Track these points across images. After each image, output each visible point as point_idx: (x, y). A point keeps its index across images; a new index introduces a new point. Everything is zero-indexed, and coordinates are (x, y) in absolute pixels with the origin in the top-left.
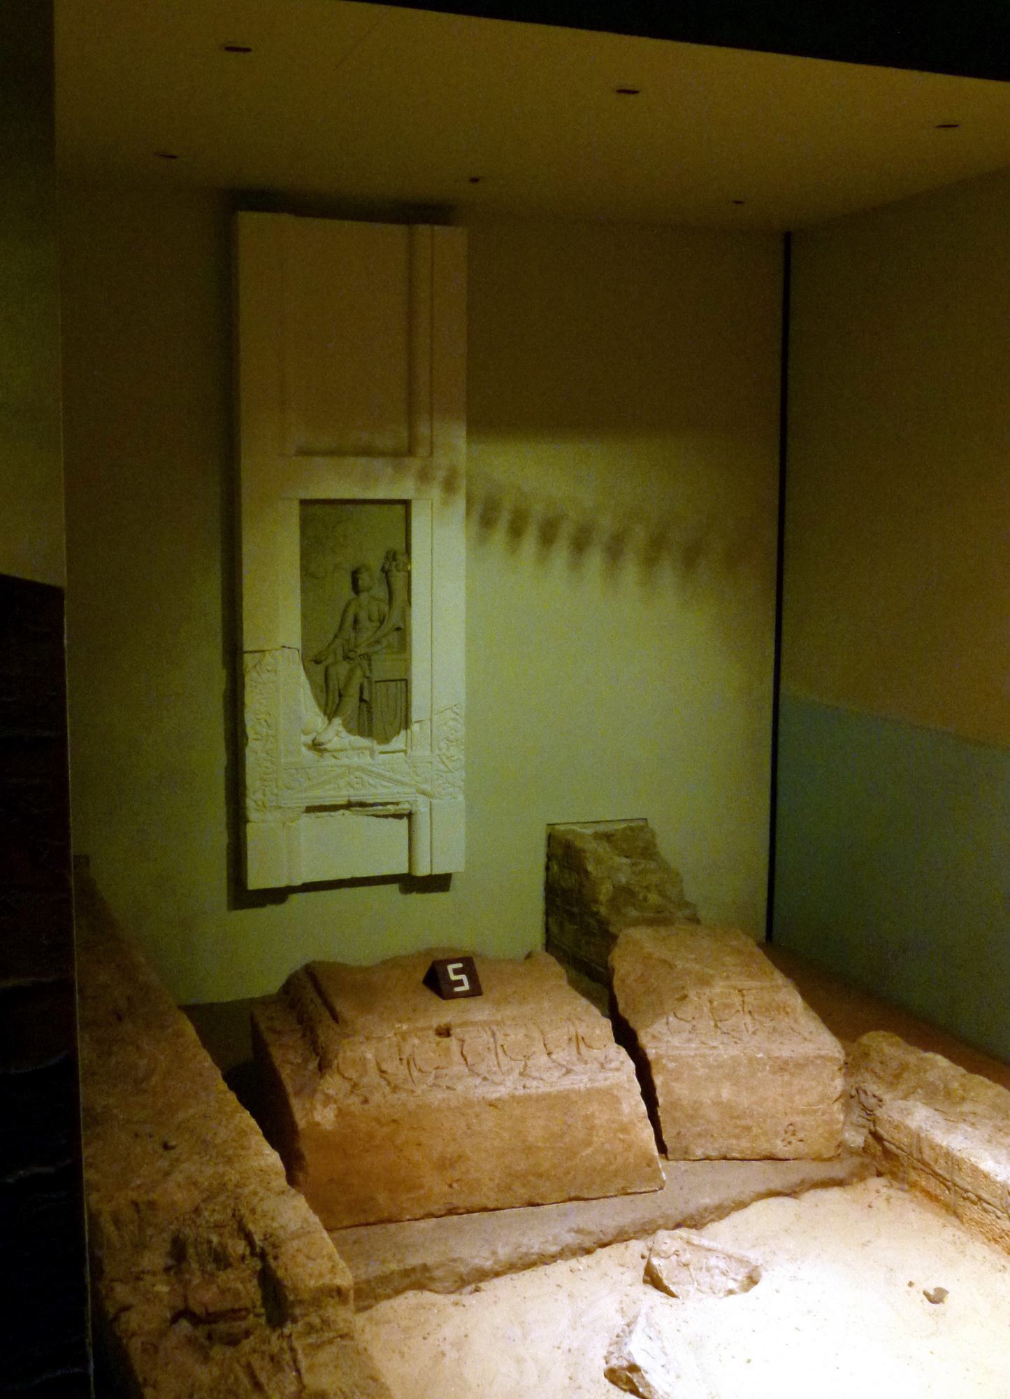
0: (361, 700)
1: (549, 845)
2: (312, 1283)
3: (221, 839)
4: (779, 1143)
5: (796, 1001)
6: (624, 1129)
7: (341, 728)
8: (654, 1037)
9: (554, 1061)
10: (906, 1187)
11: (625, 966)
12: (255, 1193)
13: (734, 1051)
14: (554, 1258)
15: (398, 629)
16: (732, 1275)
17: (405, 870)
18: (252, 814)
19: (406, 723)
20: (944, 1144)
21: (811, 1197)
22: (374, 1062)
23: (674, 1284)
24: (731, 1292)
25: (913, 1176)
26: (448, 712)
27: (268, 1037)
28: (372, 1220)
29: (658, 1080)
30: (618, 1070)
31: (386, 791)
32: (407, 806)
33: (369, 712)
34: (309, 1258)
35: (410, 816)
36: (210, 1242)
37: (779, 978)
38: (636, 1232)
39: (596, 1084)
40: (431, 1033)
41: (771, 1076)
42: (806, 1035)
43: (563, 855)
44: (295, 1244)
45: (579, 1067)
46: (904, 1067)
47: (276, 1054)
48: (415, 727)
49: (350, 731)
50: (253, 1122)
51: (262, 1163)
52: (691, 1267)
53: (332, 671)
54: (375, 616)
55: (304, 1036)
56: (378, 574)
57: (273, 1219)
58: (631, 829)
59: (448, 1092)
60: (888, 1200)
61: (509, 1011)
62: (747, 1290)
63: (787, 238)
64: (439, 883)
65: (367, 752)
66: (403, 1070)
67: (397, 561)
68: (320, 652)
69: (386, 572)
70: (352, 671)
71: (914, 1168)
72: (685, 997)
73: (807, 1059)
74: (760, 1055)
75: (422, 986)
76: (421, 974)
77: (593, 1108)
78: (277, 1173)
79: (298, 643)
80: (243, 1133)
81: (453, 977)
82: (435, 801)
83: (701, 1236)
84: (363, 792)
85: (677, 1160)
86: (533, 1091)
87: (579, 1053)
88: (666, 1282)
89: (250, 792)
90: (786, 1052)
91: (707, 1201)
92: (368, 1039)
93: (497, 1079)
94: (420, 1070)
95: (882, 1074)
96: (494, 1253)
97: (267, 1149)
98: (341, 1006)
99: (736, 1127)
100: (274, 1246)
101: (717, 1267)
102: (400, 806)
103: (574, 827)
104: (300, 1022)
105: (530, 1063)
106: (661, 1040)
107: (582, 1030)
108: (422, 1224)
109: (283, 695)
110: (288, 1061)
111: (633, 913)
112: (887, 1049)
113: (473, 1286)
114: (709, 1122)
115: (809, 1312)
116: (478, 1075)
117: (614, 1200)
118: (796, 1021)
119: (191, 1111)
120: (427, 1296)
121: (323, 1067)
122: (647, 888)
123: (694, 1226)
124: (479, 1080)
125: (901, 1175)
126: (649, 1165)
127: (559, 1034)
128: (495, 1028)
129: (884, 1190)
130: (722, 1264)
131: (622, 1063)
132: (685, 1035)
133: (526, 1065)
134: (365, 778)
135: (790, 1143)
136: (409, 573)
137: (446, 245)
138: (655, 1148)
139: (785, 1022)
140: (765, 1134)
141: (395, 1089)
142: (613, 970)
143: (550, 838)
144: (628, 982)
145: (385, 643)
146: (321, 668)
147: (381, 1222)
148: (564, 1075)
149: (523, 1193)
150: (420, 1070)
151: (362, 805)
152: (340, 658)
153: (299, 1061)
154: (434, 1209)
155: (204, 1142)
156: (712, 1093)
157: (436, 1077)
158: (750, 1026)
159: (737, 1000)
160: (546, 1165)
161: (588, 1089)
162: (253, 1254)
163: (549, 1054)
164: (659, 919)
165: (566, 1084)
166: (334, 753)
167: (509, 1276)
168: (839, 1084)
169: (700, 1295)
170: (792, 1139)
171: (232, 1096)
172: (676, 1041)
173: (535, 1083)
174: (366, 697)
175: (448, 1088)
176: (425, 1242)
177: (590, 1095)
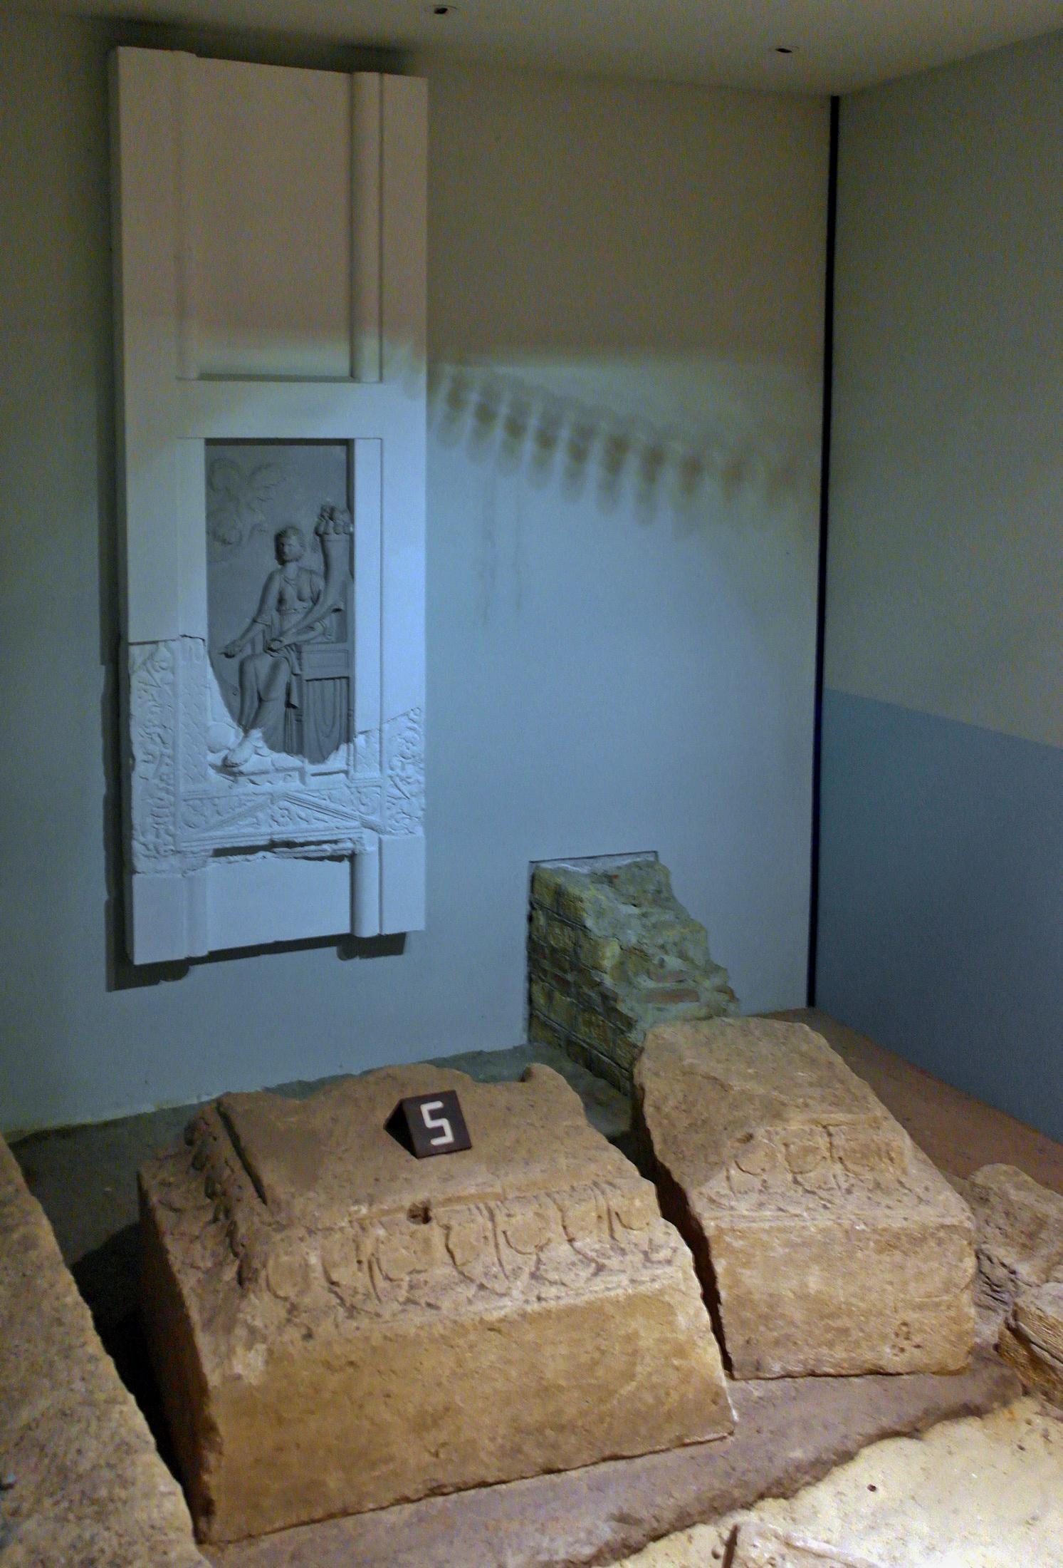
0: (289, 705)
1: (532, 889)
3: (100, 894)
5: (903, 1142)
6: (680, 1351)
7: (261, 744)
8: (712, 1201)
9: (578, 1252)
13: (825, 1220)
15: (338, 610)
18: (140, 862)
19: (348, 736)
22: (319, 1269)
26: (404, 719)
27: (164, 1218)
29: (720, 1266)
31: (321, 825)
32: (349, 845)
33: (299, 721)
35: (352, 857)
38: (702, 1513)
39: (642, 1289)
40: (402, 1216)
41: (875, 1257)
42: (920, 1191)
43: (551, 906)
45: (614, 1262)
47: (175, 1251)
48: (360, 740)
49: (273, 747)
53: (249, 668)
54: (307, 592)
55: (215, 1220)
56: (309, 536)
58: (637, 865)
61: (514, 1177)
63: (835, 102)
64: (392, 944)
65: (296, 774)
67: (336, 519)
68: (233, 643)
69: (320, 535)
70: (275, 667)
72: (750, 1137)
73: (924, 1228)
75: (385, 1134)
77: (637, 1323)
78: (178, 1529)
79: (202, 630)
80: (125, 1449)
81: (430, 1124)
82: (385, 838)
84: (291, 827)
85: (746, 1379)
86: (552, 1303)
87: (613, 1237)
89: (137, 834)
91: (798, 1454)
92: (311, 1232)
93: (499, 1286)
94: (388, 1278)
95: (1010, 1230)
98: (269, 1176)
99: (828, 1329)
102: (341, 846)
104: (211, 1195)
105: (543, 1256)
106: (722, 1204)
107: (616, 1202)
109: (182, 699)
110: (191, 1259)
111: (648, 984)
114: (792, 1323)
116: (472, 1281)
118: (904, 1172)
119: (43, 1404)
122: (663, 947)
124: (471, 1291)
126: (715, 1402)
127: (583, 1211)
128: (492, 1204)
129: (1038, 1420)
132: (754, 1198)
133: (539, 1261)
134: (294, 808)
135: (902, 1350)
136: (352, 535)
137: (399, 99)
139: (889, 1174)
140: (869, 1337)
141: (352, 1311)
142: (643, 1089)
143: (533, 879)
144: (666, 1110)
145: (319, 627)
146: (234, 663)
147: (331, 1516)
148: (595, 1274)
149: (539, 1457)
150: (388, 1278)
151: (289, 844)
152: (259, 648)
153: (209, 1264)
155: (63, 1472)
156: (794, 1283)
157: (412, 1287)
158: (841, 1179)
159: (822, 1141)
160: (571, 1411)
161: (629, 1298)
163: (571, 1241)
166: (252, 777)
170: (905, 1344)
171: (108, 1365)
172: (743, 1207)
173: (553, 1291)
174: (295, 701)
177: (631, 1305)
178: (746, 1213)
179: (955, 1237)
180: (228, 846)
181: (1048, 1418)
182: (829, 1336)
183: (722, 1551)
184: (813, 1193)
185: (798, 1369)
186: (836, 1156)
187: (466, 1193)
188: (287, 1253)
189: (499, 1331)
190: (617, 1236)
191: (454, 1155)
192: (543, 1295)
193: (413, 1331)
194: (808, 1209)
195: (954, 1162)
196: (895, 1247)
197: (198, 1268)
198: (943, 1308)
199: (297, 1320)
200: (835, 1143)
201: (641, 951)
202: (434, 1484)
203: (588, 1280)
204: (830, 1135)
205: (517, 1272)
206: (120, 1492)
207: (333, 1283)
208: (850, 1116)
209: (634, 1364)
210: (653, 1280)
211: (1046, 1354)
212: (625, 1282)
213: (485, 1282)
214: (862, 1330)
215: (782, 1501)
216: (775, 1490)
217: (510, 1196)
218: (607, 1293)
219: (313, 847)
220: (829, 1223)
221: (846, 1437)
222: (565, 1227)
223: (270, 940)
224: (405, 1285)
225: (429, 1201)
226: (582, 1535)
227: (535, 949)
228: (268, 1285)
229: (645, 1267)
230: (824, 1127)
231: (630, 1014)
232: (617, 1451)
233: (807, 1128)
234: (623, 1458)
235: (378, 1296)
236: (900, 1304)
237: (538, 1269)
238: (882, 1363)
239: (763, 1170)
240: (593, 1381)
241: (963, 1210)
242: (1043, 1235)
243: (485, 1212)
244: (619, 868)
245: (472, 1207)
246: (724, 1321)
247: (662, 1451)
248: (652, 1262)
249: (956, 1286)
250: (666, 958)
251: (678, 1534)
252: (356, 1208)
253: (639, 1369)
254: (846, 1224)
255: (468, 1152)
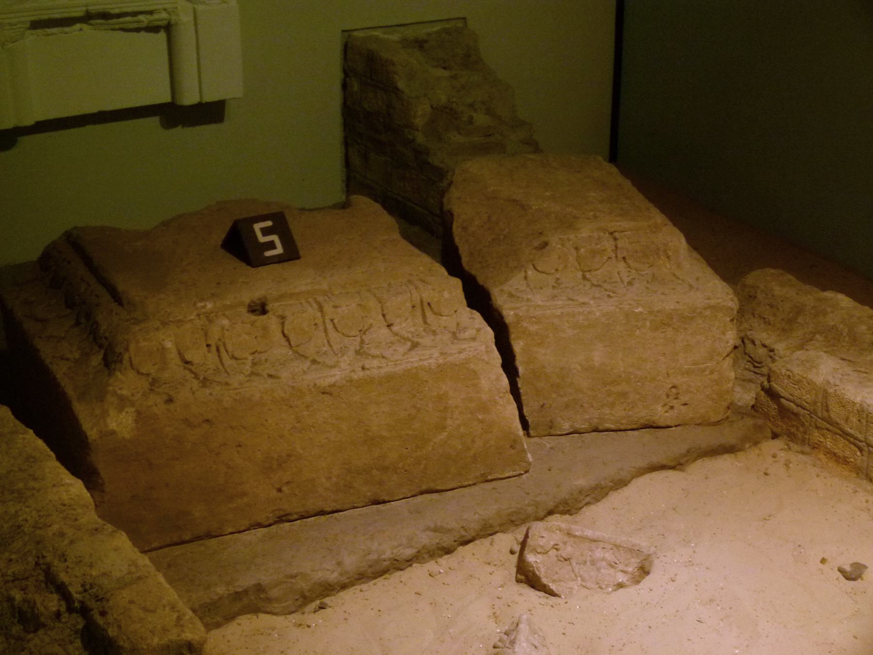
2: (156, 641)
4: (659, 408)
5: (677, 241)
6: (484, 408)
8: (511, 295)
10: (807, 449)
11: (466, 211)
12: (62, 535)
14: (409, 562)
16: (621, 567)
17: (166, 98)
20: (858, 400)
21: (699, 468)
22: (174, 351)
23: (554, 581)
24: (620, 586)
25: (816, 436)
28: (187, 538)
29: (518, 346)
30: (474, 339)
32: (164, 15)
34: (146, 610)
35: (168, 28)
36: (10, 599)
37: (659, 218)
38: (501, 525)
40: (244, 310)
43: (365, 72)
44: (126, 595)
45: (426, 340)
46: (799, 310)
47: (46, 351)
50: (40, 443)
51: (65, 496)
52: (574, 562)
55: (78, 324)
57: (91, 566)
58: (447, 31)
59: (270, 381)
60: (787, 465)
62: (638, 582)
64: (210, 113)
66: (212, 358)
71: (817, 428)
72: (546, 244)
74: (640, 309)
75: (222, 252)
76: (219, 235)
81: (262, 239)
83: (576, 523)
85: (540, 436)
86: (375, 372)
87: (425, 322)
88: (545, 581)
90: (669, 305)
91: (581, 482)
92: (164, 324)
94: (233, 357)
95: (772, 319)
96: (339, 564)
97: (68, 478)
100: (99, 599)
101: (603, 559)
102: (156, 16)
103: (375, 33)
105: (366, 338)
107: (427, 294)
108: (247, 537)
110: (62, 356)
111: (456, 138)
112: (778, 291)
113: (318, 602)
115: (711, 600)
116: (306, 358)
117: (473, 489)
118: (679, 266)
120: (264, 620)
121: (111, 360)
122: (471, 106)
123: (568, 512)
124: (308, 363)
125: (800, 436)
128: (320, 299)
130: (609, 556)
131: (479, 330)
133: (362, 342)
135: (672, 407)
138: (519, 426)
141: (205, 382)
142: (452, 215)
143: (346, 48)
147: (199, 538)
150: (233, 357)
151: (105, 16)
153: (77, 355)
154: (262, 518)
157: (254, 364)
159: (608, 244)
162: (70, 610)
164: (489, 146)
165: (414, 360)
167: (358, 587)
168: (731, 337)
169: (585, 592)
170: (674, 403)
172: (538, 299)
173: (376, 363)
175: (270, 376)
176: (250, 554)
178: (540, 303)
179: (720, 315)
180: (45, 17)
181: (790, 452)
182: (611, 399)
183: (517, 548)
184: (598, 286)
185: (585, 426)
186: (620, 256)
187: (297, 290)
188: (144, 340)
189: (331, 394)
190: (429, 321)
191: (286, 264)
192: (367, 366)
193: (258, 396)
194: (594, 298)
195: (729, 269)
196: (669, 325)
197: (67, 359)
198: (707, 372)
199: (160, 390)
200: (619, 246)
201: (452, 109)
202: (282, 513)
203: (405, 354)
204: (615, 239)
205: (343, 351)
206: (32, 484)
207: (187, 362)
208: (632, 223)
209: (445, 419)
210: (460, 353)
211: (792, 404)
212: (436, 355)
213: (317, 358)
214: (638, 393)
215: (567, 516)
216: (561, 508)
217: (337, 292)
218: (421, 363)
219: (128, 19)
220: (612, 308)
221: (622, 469)
222: (384, 316)
223: (95, 110)
224: (249, 363)
225: (265, 298)
226: (404, 541)
227: (350, 114)
228: (131, 365)
229: (453, 343)
230: (611, 234)
231: (442, 165)
232: (432, 485)
233: (595, 235)
234: (437, 491)
235: (226, 371)
236: (671, 372)
237: (362, 348)
238: (655, 418)
239: (557, 270)
240: (411, 432)
241: (728, 293)
242: (800, 320)
243: (315, 306)
244: (429, 34)
245: (303, 301)
246: (521, 391)
247: (470, 485)
248: (460, 340)
249: (719, 354)
250: (475, 115)
251: (483, 540)
252: (203, 304)
253: (449, 422)
254: (626, 307)
255: (297, 261)
